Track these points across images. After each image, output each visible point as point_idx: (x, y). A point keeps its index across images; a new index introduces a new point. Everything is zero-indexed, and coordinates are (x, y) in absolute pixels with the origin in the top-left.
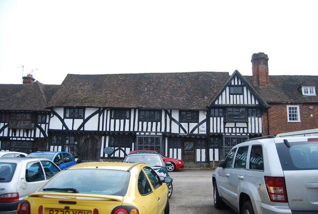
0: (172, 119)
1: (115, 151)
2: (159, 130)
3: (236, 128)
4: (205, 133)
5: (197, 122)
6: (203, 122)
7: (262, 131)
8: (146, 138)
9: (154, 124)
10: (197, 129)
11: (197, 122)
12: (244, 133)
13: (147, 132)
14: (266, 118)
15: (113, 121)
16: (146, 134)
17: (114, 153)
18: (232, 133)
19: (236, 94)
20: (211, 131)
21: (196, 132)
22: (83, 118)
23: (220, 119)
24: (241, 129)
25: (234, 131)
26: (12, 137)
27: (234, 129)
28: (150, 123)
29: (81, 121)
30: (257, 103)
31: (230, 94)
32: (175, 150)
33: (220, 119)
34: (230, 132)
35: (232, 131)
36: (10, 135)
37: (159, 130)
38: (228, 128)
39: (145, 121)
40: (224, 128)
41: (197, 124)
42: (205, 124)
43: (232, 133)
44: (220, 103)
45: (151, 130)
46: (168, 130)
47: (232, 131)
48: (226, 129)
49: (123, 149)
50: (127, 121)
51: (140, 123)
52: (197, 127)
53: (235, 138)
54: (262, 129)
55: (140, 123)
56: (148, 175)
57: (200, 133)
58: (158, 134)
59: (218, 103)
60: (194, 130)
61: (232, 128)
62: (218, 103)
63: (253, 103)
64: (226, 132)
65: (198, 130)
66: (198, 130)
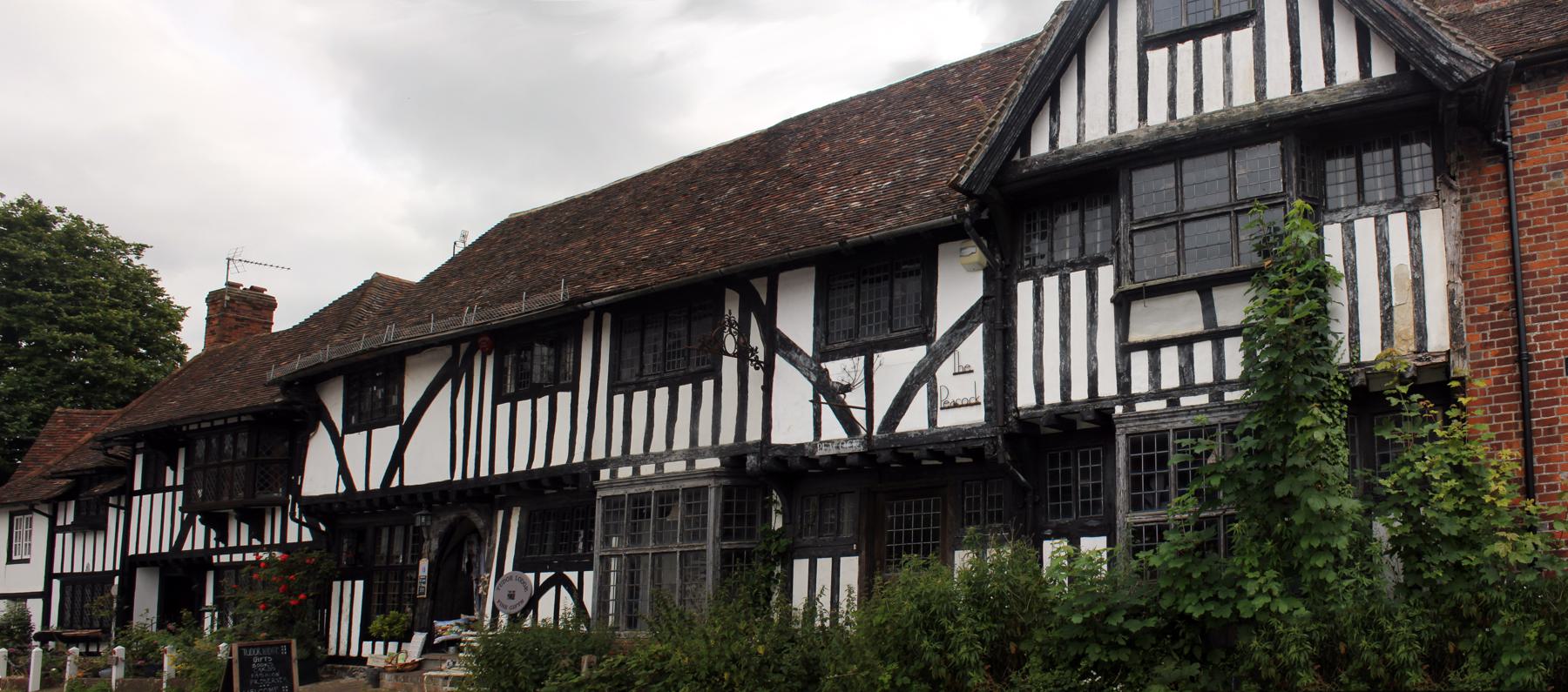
0: (778, 343)
1: (540, 590)
2: (705, 440)
3: (1216, 336)
4: (977, 416)
5: (923, 335)
6: (962, 328)
7: (1455, 336)
8: (1149, 437)
9: (685, 391)
10: (923, 391)
11: (923, 335)
12: (1188, 387)
13: (670, 452)
14: (1494, 206)
15: (504, 409)
16: (1186, 401)
17: (532, 604)
18: (670, 452)
19: (1197, 33)
20: (1025, 397)
21: (914, 421)
22: (397, 419)
23: (1092, 285)
24: (1170, 357)
25: (1203, 372)
26: (219, 551)
27: (1203, 351)
28: (662, 394)
29: (915, 355)
30: (1382, 66)
31: (1147, 42)
32: (824, 565)
33: (1092, 285)
34: (1170, 379)
35: (1186, 369)
36: (213, 545)
37: (705, 440)
38: (1154, 347)
39: (640, 389)
40: (1125, 349)
41: (919, 352)
42: (973, 348)
43: (1188, 387)
44: (1067, 140)
45: (669, 442)
46: (754, 434)
47: (1186, 369)
48: (1140, 361)
49: (573, 576)
50: (564, 398)
51: (756, 377)
52: (923, 375)
53: (1210, 431)
54: (1453, 311)
55: (619, 400)
56: (117, 681)
57: (946, 420)
58: (1141, 407)
59: (1053, 141)
60: (901, 403)
61: (1185, 343)
62: (1053, 141)
63: (1348, 70)
64: (1140, 384)
65: (933, 396)
66: (933, 396)
